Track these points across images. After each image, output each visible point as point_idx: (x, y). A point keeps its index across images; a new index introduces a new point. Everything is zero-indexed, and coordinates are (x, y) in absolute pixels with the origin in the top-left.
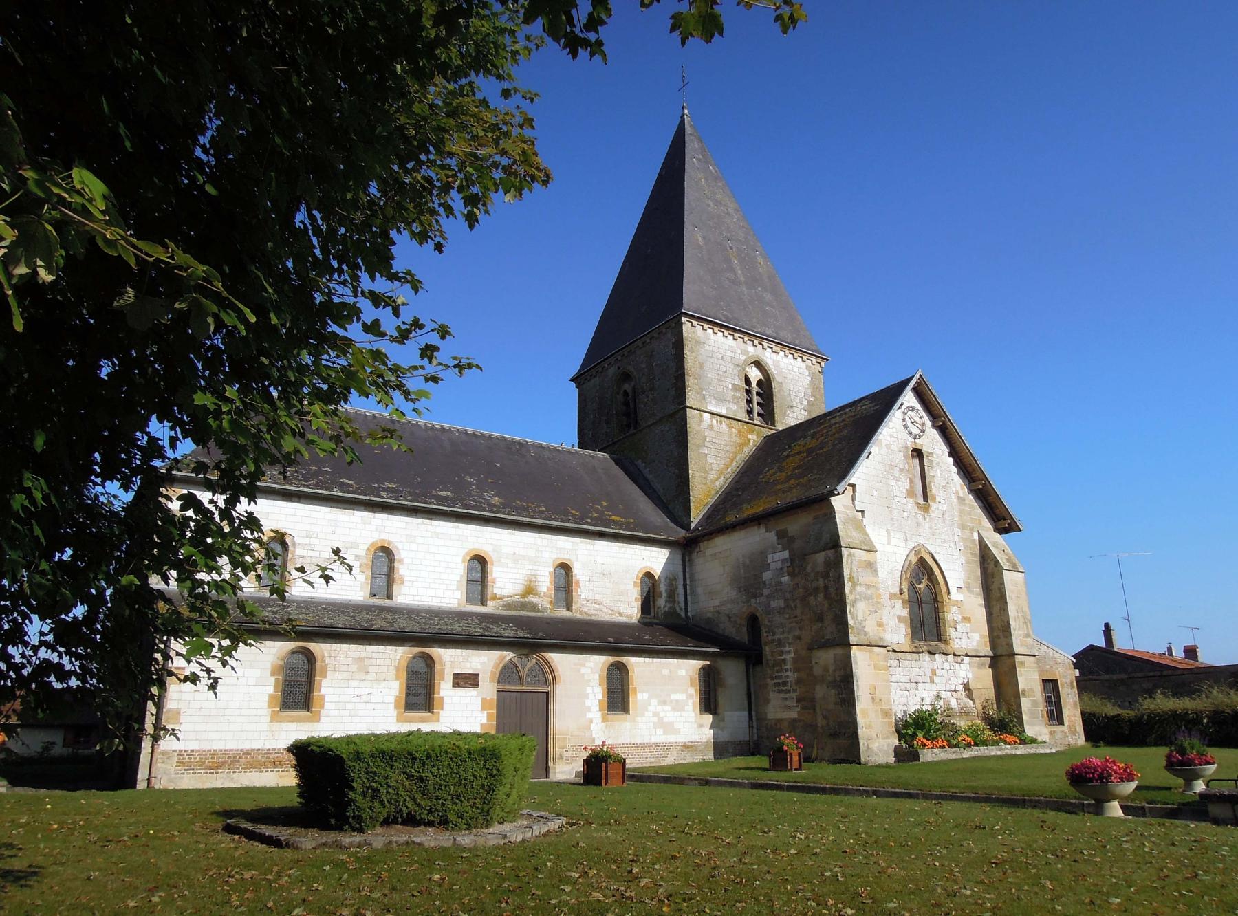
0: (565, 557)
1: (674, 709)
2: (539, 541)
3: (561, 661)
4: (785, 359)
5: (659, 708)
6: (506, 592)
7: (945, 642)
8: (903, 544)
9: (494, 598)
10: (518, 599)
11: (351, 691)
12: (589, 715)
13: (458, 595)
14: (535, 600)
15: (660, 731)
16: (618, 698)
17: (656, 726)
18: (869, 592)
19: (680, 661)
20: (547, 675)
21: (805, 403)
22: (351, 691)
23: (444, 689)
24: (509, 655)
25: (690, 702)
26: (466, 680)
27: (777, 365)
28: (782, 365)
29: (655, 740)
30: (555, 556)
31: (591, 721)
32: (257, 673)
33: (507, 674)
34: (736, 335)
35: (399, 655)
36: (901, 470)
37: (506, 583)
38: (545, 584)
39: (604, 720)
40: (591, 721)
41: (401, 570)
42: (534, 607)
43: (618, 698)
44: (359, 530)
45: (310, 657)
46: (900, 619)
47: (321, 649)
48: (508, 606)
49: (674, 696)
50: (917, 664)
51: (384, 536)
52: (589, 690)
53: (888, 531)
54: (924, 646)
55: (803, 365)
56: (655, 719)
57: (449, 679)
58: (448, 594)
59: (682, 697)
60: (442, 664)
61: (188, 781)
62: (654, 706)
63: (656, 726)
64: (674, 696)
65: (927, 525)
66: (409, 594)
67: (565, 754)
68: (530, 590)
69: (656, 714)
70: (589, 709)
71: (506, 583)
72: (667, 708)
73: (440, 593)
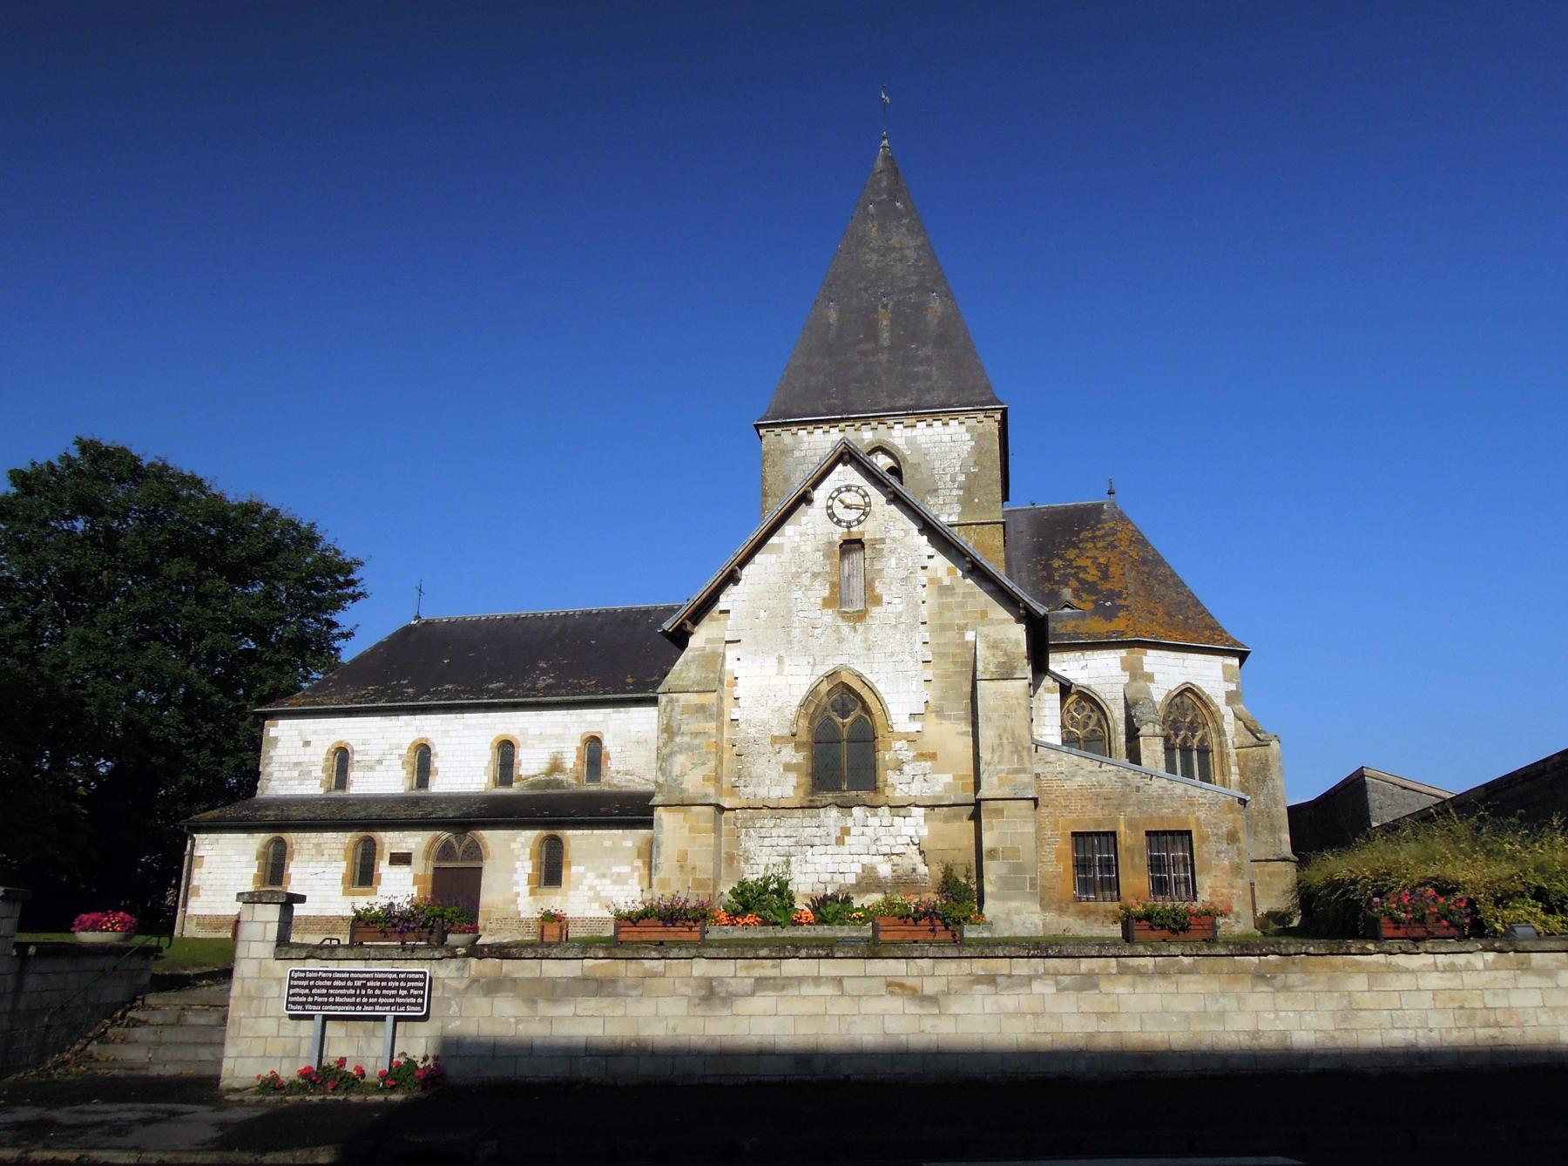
0: (594, 730)
1: (615, 883)
2: (567, 718)
3: (491, 838)
4: (930, 431)
5: (597, 882)
6: (531, 773)
7: (875, 789)
8: (808, 670)
9: (520, 778)
10: (542, 777)
11: (310, 870)
12: (516, 889)
13: (485, 780)
14: (560, 777)
15: (596, 906)
16: (551, 871)
17: (591, 900)
18: (697, 741)
19: (627, 832)
20: (476, 852)
21: (962, 478)
22: (310, 870)
23: (383, 868)
24: (445, 835)
25: (636, 874)
26: (401, 859)
27: (911, 442)
28: (921, 440)
29: (589, 914)
30: (583, 730)
31: (518, 894)
32: (247, 858)
33: (445, 851)
34: (842, 425)
35: (345, 839)
36: (815, 575)
37: (531, 764)
38: (572, 759)
39: (532, 893)
40: (518, 894)
41: (436, 763)
42: (559, 784)
43: (551, 871)
44: (403, 730)
45: (281, 842)
46: (788, 768)
47: (291, 837)
48: (533, 785)
49: (615, 869)
50: (815, 822)
51: (423, 735)
52: (518, 864)
53: (780, 660)
54: (829, 797)
55: (964, 428)
56: (591, 893)
57: (387, 858)
58: (476, 780)
59: (627, 869)
60: (382, 844)
61: (201, 935)
62: (591, 878)
63: (591, 900)
64: (615, 869)
65: (858, 639)
66: (362, 784)
67: (489, 926)
68: (556, 767)
69: (592, 888)
70: (517, 883)
71: (531, 764)
72: (607, 881)
73: (468, 780)
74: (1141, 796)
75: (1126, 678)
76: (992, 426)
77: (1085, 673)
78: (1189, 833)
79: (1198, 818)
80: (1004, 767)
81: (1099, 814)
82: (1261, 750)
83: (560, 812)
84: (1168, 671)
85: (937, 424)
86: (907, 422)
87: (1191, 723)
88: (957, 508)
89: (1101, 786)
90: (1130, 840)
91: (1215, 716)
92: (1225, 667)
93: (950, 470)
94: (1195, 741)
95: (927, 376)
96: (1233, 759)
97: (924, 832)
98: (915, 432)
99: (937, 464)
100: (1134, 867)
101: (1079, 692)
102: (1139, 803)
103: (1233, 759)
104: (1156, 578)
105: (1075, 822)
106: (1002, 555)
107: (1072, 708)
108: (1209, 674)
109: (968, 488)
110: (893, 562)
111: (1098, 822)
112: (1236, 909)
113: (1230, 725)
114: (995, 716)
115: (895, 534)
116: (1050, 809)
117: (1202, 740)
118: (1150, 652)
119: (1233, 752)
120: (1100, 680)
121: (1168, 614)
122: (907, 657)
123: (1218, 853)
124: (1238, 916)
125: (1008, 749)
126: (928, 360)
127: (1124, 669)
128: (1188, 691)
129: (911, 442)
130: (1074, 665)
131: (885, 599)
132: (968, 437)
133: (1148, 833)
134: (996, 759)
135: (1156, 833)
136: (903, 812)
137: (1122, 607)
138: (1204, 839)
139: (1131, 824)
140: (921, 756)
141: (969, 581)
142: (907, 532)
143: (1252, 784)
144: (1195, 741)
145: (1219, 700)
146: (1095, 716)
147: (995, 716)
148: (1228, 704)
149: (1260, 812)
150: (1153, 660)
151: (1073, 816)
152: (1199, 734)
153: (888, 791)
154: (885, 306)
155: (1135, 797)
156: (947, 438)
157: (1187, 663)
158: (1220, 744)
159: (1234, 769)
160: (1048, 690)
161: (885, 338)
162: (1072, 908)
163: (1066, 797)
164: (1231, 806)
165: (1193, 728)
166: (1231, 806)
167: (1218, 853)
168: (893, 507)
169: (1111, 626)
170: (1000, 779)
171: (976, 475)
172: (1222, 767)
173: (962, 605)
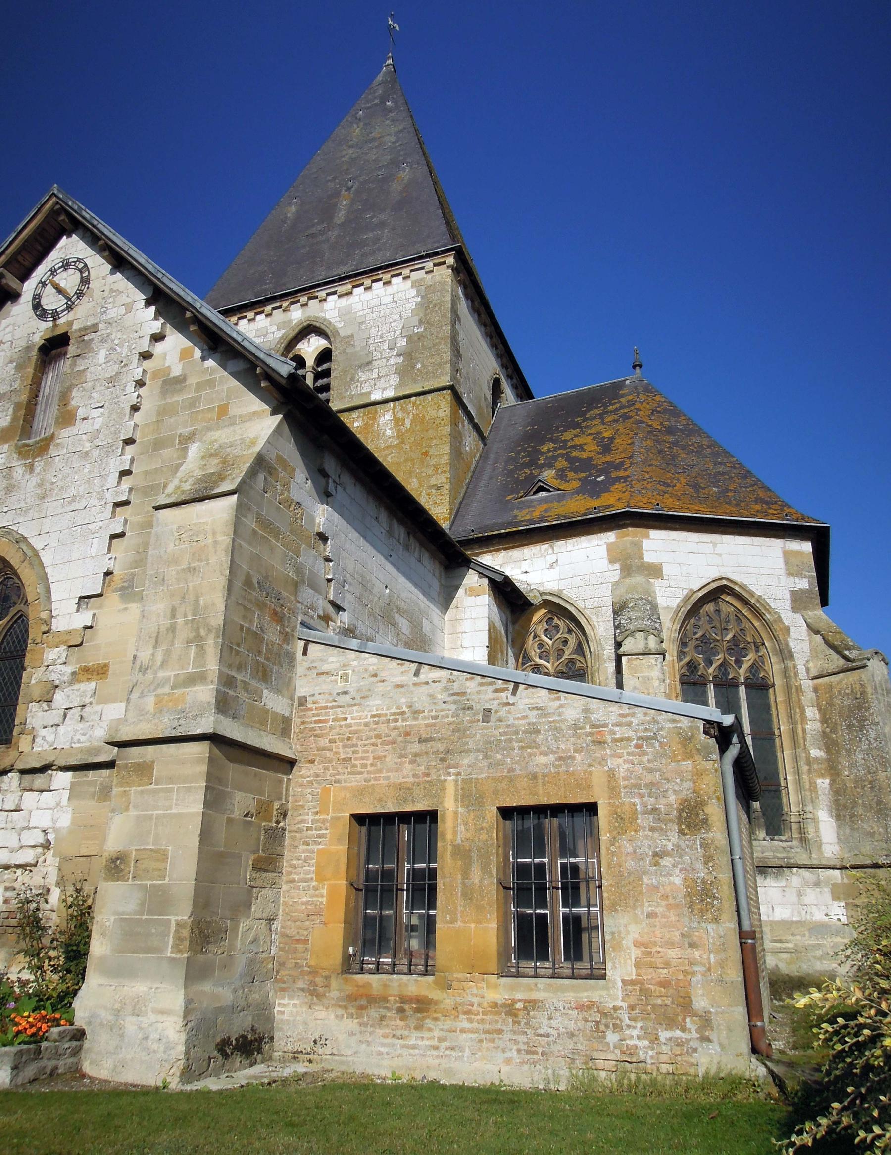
4: (369, 295)
21: (403, 342)
34: (268, 309)
55: (409, 283)
74: (493, 730)
75: (614, 573)
76: (442, 274)
77: (554, 574)
78: (591, 808)
79: (611, 775)
80: (168, 673)
81: (407, 773)
82: (851, 678)
83: (317, 813)
84: (684, 562)
85: (377, 286)
86: (341, 289)
87: (735, 641)
88: (394, 380)
89: (416, 713)
90: (469, 838)
91: (775, 631)
92: (787, 554)
93: (389, 336)
94: (742, 671)
95: (377, 239)
96: (808, 696)
97: (65, 820)
98: (352, 300)
99: (373, 332)
100: (467, 894)
101: (546, 603)
102: (488, 747)
103: (808, 696)
104: (683, 448)
105: (360, 792)
106: (448, 429)
107: (540, 630)
108: (767, 568)
109: (408, 355)
110: (103, 353)
111: (404, 790)
112: (700, 1003)
113: (800, 641)
114: (171, 572)
115: (113, 313)
116: (317, 768)
117: (755, 668)
118: (655, 534)
119: (808, 685)
120: (577, 581)
121: (696, 486)
122: (94, 501)
123: (658, 855)
124: (706, 1022)
125: (184, 633)
126: (382, 225)
127: (611, 561)
128: (720, 591)
129: (345, 314)
130: (540, 563)
131: (81, 413)
132: (414, 292)
133: (506, 813)
134: (159, 658)
135: (522, 812)
136: (39, 780)
137: (618, 479)
138: (625, 822)
139: (470, 796)
140: (88, 672)
141: (211, 363)
142: (129, 308)
143: (843, 735)
144: (742, 671)
145: (779, 602)
146: (572, 640)
147: (171, 572)
148: (794, 609)
149: (858, 781)
150: (658, 544)
151: (355, 781)
152: (749, 659)
153: (24, 743)
154: (349, 189)
155: (479, 733)
156: (387, 299)
157: (720, 548)
158: (785, 671)
159: (811, 713)
160: (472, 592)
161: (341, 216)
162: (337, 988)
163: (348, 741)
164: (687, 740)
165: (737, 649)
166: (687, 740)
167: (658, 855)
168: (119, 275)
169: (597, 503)
170: (159, 700)
171: (420, 337)
172: (789, 709)
173: (192, 403)
